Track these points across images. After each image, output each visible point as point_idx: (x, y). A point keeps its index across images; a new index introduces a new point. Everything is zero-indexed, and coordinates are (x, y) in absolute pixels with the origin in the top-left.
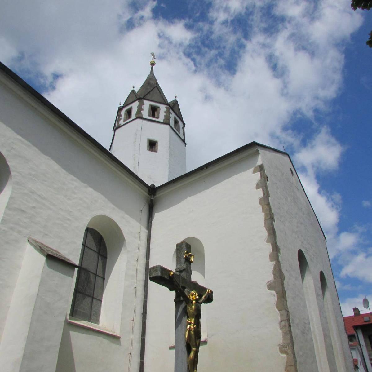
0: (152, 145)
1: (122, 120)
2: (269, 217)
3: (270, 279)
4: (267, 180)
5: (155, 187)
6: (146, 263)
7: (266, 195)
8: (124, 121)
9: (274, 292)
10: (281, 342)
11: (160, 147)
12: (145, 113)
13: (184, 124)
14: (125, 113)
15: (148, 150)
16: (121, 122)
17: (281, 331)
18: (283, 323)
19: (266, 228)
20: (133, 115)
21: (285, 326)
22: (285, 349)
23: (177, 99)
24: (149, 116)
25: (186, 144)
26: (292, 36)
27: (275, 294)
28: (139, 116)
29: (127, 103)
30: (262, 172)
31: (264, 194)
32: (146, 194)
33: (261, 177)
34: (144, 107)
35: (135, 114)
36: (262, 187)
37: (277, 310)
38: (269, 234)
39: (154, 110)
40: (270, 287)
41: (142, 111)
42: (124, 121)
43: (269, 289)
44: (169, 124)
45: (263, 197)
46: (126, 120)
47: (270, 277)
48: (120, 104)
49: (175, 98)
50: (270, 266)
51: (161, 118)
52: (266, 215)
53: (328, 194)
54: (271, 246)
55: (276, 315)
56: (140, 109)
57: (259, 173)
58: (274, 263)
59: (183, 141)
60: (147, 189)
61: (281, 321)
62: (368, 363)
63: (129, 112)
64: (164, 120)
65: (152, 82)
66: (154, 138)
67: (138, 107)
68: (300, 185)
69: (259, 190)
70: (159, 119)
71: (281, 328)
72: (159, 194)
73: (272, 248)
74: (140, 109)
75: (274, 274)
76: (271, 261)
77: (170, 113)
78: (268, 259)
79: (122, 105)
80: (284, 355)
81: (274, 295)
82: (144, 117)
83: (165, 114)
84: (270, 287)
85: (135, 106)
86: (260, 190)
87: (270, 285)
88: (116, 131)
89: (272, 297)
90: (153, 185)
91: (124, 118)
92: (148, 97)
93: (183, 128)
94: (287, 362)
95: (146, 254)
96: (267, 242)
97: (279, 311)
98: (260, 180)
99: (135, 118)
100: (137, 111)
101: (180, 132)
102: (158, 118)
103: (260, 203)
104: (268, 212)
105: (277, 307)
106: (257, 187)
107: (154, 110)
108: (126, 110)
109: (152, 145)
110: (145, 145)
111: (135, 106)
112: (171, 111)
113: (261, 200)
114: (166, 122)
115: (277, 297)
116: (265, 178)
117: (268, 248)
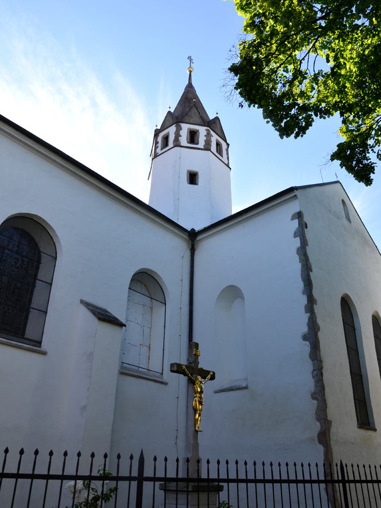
2: (305, 268)
3: (304, 331)
4: (305, 227)
5: (195, 231)
7: (304, 243)
8: (162, 149)
9: (307, 343)
10: (313, 390)
12: (184, 140)
13: (228, 145)
14: (162, 140)
16: (159, 151)
17: (313, 380)
18: (315, 372)
19: (302, 279)
20: (171, 144)
21: (317, 375)
22: (316, 396)
23: (218, 116)
24: (188, 143)
25: (230, 169)
26: (299, 215)
28: (177, 144)
29: (164, 126)
30: (300, 219)
31: (301, 243)
33: (299, 224)
34: (181, 133)
35: (173, 141)
36: (299, 236)
37: (310, 360)
38: (305, 286)
39: (193, 137)
40: (305, 338)
41: (180, 138)
42: (162, 149)
43: (304, 340)
44: (210, 150)
45: (301, 246)
46: (164, 148)
47: (305, 329)
48: (157, 126)
49: (216, 116)
50: (305, 317)
51: (201, 144)
52: (303, 266)
55: (309, 366)
56: (177, 135)
57: (297, 220)
58: (309, 314)
59: (228, 165)
60: (185, 236)
61: (314, 370)
62: (378, 497)
63: (166, 138)
64: (204, 146)
65: (190, 96)
66: (194, 169)
67: (175, 133)
68: (344, 192)
69: (297, 238)
70: (199, 145)
71: (313, 377)
73: (308, 300)
74: (177, 135)
75: (308, 326)
76: (306, 312)
77: (211, 136)
78: (303, 310)
79: (159, 127)
80: (315, 402)
81: (308, 346)
84: (305, 338)
85: (172, 130)
86: (298, 239)
87: (304, 335)
89: (306, 347)
90: (193, 230)
91: (161, 145)
93: (227, 150)
94: (317, 408)
96: (303, 293)
97: (312, 361)
98: (298, 228)
100: (174, 138)
101: (223, 155)
102: (197, 144)
103: (298, 253)
104: (305, 263)
105: (310, 358)
106: (295, 236)
107: (193, 137)
111: (172, 130)
112: (212, 132)
113: (298, 249)
114: (207, 148)
115: (311, 348)
116: (303, 226)
117: (304, 300)
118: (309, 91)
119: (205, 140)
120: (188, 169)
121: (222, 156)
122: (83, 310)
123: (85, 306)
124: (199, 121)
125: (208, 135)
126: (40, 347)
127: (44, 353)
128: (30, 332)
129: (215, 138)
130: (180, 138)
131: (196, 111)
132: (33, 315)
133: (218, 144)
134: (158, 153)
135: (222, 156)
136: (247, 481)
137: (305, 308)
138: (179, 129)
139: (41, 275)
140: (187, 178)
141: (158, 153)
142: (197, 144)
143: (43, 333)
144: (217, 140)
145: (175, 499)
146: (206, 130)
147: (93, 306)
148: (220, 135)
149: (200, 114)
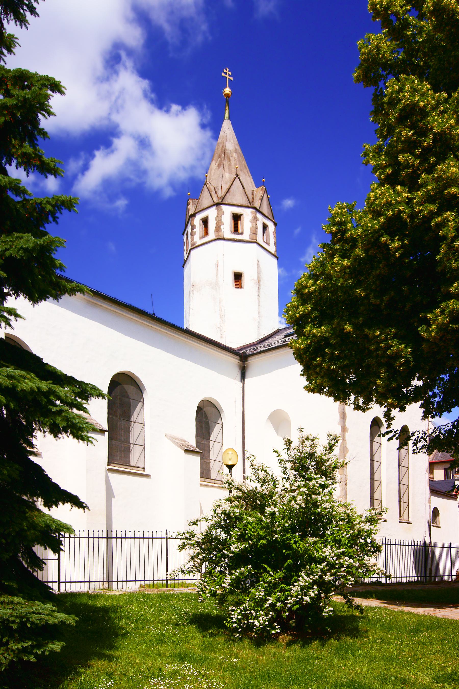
1: (197, 233)
60: (234, 361)
63: (205, 222)
66: (239, 270)
72: (253, 362)
82: (226, 236)
88: (192, 252)
99: (214, 237)
102: (242, 233)
112: (259, 216)
121: (268, 244)
126: (144, 470)
127: (148, 476)
128: (134, 458)
133: (265, 227)
142: (242, 233)
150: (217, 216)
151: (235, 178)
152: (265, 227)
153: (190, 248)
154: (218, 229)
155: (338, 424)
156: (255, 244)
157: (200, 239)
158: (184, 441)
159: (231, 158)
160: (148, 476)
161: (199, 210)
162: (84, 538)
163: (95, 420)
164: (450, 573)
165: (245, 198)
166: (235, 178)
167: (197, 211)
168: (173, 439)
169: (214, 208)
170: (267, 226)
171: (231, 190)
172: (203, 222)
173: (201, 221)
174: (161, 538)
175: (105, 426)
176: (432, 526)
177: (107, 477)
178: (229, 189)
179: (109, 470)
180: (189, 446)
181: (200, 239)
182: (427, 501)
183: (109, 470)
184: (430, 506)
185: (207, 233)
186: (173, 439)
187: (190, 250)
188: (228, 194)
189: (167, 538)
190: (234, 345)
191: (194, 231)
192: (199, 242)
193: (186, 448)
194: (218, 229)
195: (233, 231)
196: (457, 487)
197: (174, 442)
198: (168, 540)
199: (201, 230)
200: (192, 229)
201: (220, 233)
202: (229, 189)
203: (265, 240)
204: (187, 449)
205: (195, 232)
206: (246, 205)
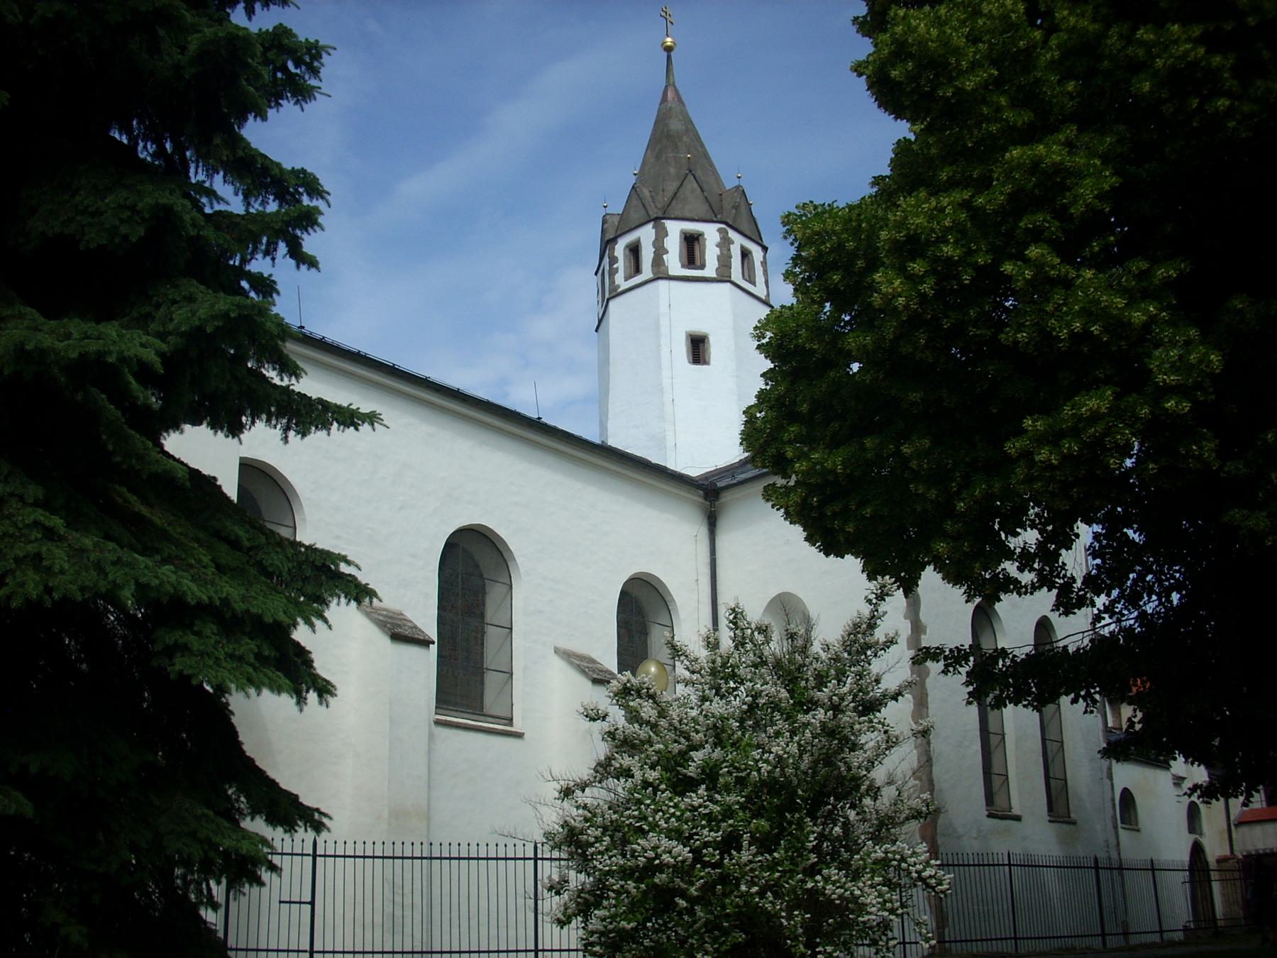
0: (698, 348)
1: (620, 271)
6: (711, 562)
8: (626, 279)
11: (716, 350)
12: (674, 263)
15: (689, 362)
21: (921, 745)
24: (683, 266)
27: (912, 700)
28: (661, 274)
32: (701, 500)
41: (665, 257)
46: (631, 277)
51: (710, 270)
53: (223, 686)
54: (910, 624)
56: (660, 251)
60: (698, 498)
63: (634, 250)
66: (699, 328)
72: (726, 497)
77: (730, 242)
82: (671, 273)
83: (718, 250)
85: (646, 235)
88: (611, 303)
92: (676, 209)
95: (711, 616)
99: (651, 276)
102: (702, 267)
108: (627, 246)
109: (698, 348)
110: (681, 349)
112: (732, 234)
114: (723, 277)
115: (914, 704)
118: (870, 678)
119: (718, 256)
120: (688, 330)
121: (754, 283)
122: (558, 664)
123: (563, 658)
124: (703, 210)
125: (725, 243)
126: (512, 726)
127: (519, 736)
128: (491, 700)
129: (738, 240)
130: (665, 257)
131: (695, 185)
132: (491, 680)
133: (745, 254)
134: (619, 286)
135: (754, 283)
136: (996, 939)
137: (908, 641)
138: (661, 234)
139: (490, 615)
140: (688, 350)
141: (619, 286)
142: (702, 267)
143: (512, 705)
144: (742, 248)
145: (1272, 817)
146: (719, 230)
147: (582, 658)
148: (748, 233)
149: (703, 191)
150: (656, 239)
151: (687, 175)
152: (745, 254)
153: (607, 296)
154: (658, 261)
155: (905, 618)
156: (729, 284)
157: (625, 281)
158: (594, 661)
159: (679, 144)
160: (519, 736)
161: (623, 231)
162: (364, 857)
163: (411, 622)
164: (1157, 926)
165: (706, 207)
166: (687, 175)
167: (619, 233)
168: (568, 656)
169: (650, 225)
170: (750, 252)
171: (678, 194)
172: (630, 250)
173: (628, 250)
174: (524, 859)
175: (432, 632)
176: (1122, 828)
177: (431, 737)
178: (676, 193)
179: (438, 723)
180: (601, 671)
181: (625, 281)
182: (1105, 775)
183: (536, 844)
184: (1112, 785)
185: (637, 270)
186: (568, 656)
187: (608, 300)
188: (674, 202)
189: (536, 859)
190: (694, 472)
191: (615, 266)
192: (624, 285)
193: (595, 676)
194: (658, 261)
195: (686, 263)
196: (198, 197)
197: (571, 664)
198: (539, 862)
199: (627, 264)
200: (611, 264)
201: (662, 268)
202: (676, 193)
203: (747, 277)
204: (599, 677)
205: (617, 268)
206: (709, 218)
